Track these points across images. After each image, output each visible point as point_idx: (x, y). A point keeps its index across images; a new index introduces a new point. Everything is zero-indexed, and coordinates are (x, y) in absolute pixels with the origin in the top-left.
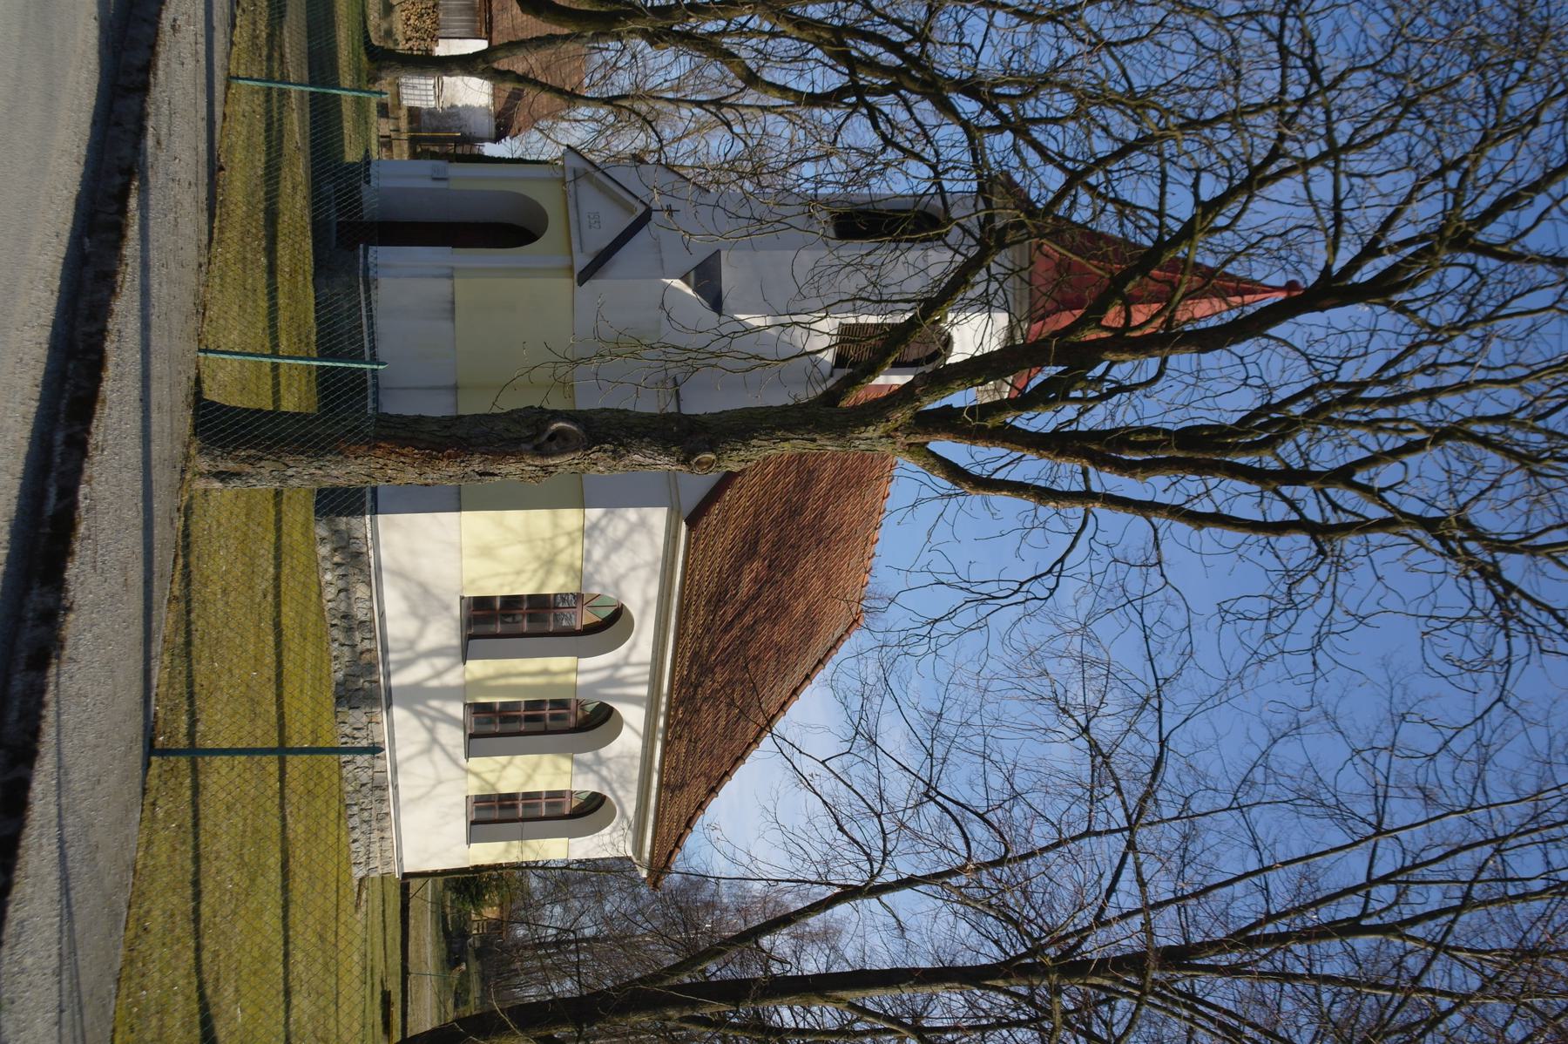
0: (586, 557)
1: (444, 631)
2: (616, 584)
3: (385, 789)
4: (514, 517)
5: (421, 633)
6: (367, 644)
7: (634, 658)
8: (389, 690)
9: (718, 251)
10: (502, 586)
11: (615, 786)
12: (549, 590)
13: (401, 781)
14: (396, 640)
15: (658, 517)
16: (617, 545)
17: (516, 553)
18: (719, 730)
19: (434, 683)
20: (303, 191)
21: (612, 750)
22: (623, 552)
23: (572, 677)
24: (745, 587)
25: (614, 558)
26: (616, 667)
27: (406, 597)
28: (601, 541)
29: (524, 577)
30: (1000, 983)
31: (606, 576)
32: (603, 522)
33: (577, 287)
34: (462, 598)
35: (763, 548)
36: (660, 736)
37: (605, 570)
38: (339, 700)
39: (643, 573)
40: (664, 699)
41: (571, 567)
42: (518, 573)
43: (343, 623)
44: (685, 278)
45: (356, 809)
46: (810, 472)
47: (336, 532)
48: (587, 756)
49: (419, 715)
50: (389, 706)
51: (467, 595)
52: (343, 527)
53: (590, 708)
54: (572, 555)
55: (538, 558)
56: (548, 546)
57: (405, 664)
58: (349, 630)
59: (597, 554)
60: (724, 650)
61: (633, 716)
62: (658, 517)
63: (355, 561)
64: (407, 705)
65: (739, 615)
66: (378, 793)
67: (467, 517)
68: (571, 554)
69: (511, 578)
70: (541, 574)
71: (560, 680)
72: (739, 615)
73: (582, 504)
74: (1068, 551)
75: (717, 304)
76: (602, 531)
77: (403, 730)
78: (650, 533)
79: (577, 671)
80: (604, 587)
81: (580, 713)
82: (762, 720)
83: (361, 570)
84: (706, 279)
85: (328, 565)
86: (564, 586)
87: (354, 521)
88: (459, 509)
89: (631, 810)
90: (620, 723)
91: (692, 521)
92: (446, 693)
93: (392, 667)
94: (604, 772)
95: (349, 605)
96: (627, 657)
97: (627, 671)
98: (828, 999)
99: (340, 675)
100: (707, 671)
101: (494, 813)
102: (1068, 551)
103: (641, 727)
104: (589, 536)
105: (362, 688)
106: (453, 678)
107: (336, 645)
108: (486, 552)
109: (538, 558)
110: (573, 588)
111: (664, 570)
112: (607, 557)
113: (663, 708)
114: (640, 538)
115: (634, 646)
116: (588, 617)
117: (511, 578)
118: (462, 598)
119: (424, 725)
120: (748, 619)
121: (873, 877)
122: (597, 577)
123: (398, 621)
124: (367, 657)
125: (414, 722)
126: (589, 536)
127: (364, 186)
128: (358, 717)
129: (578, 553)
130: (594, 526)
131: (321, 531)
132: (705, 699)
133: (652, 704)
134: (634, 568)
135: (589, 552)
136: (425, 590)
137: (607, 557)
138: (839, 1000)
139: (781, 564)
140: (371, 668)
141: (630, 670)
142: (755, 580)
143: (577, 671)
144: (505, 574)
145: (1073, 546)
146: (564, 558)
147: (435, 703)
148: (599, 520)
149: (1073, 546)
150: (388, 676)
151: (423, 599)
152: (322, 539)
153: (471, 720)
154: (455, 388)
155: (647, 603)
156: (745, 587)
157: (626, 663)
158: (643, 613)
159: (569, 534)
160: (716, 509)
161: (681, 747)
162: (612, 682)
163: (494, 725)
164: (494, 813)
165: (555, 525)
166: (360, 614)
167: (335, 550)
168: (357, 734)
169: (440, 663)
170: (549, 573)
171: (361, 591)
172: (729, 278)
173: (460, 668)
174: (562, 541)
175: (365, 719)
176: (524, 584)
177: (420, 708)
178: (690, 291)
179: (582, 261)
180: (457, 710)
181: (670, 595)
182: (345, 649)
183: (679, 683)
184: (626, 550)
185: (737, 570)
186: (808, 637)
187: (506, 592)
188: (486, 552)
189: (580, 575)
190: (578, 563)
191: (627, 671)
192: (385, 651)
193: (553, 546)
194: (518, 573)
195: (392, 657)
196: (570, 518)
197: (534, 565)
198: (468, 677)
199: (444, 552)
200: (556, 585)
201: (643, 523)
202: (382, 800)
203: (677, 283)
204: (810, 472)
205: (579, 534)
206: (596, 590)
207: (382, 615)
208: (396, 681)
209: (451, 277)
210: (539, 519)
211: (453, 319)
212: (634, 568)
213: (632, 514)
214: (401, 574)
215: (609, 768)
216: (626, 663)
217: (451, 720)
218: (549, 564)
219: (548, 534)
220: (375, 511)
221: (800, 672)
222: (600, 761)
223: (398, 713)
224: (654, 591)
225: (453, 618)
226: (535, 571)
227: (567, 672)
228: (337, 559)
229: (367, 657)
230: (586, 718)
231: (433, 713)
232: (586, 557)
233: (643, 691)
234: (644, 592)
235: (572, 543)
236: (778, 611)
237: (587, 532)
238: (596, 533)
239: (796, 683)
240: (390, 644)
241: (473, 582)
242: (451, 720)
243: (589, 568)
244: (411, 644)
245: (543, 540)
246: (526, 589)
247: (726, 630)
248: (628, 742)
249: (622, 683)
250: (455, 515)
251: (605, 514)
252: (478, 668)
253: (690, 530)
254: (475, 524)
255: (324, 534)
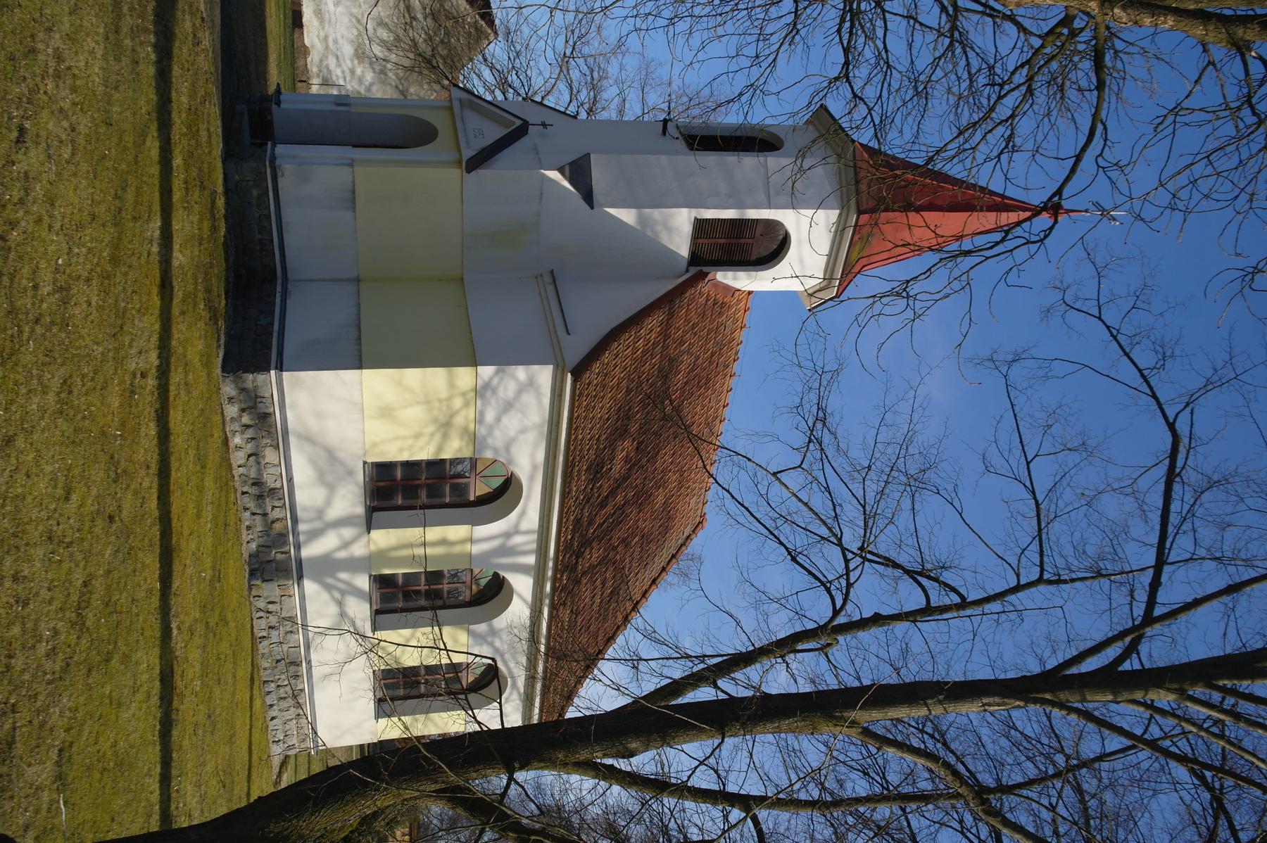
0: (480, 419)
1: (349, 500)
2: (507, 448)
3: (299, 664)
4: (413, 376)
5: (328, 502)
6: (277, 514)
7: (524, 526)
8: (299, 562)
9: (589, 154)
10: (401, 450)
11: (507, 656)
12: (447, 455)
13: (313, 657)
14: (305, 509)
15: (544, 375)
16: (508, 406)
17: (414, 414)
18: (595, 607)
19: (342, 554)
20: (208, 40)
21: (500, 622)
22: (513, 413)
23: (468, 547)
24: (618, 467)
25: (505, 420)
26: (507, 535)
27: (313, 461)
28: (493, 402)
29: (423, 440)
30: (1048, 696)
31: (497, 440)
32: (495, 381)
33: (465, 174)
34: (365, 463)
35: (634, 428)
36: (547, 601)
37: (497, 433)
38: (252, 574)
39: (531, 437)
40: (551, 564)
41: (465, 430)
42: (417, 436)
43: (254, 490)
44: (561, 170)
45: (273, 685)
46: (671, 361)
47: (243, 390)
48: (481, 628)
49: (328, 588)
50: (300, 578)
51: (369, 460)
52: (249, 385)
53: (483, 582)
54: (466, 418)
55: (435, 420)
56: (444, 408)
57: (315, 534)
58: (260, 497)
59: (490, 416)
60: (601, 525)
61: (522, 585)
62: (544, 375)
63: (263, 422)
64: (318, 579)
65: (613, 493)
66: (292, 669)
67: (367, 373)
68: (465, 417)
69: (410, 442)
70: (438, 437)
71: (457, 549)
72: (613, 493)
73: (474, 362)
74: (1068, 179)
75: (588, 198)
76: (494, 391)
77: (316, 602)
78: (539, 395)
79: (471, 540)
80: (496, 450)
81: (474, 587)
82: (629, 606)
83: (269, 433)
84: (579, 172)
85: (236, 427)
86: (460, 450)
87: (261, 378)
88: (360, 367)
89: (521, 683)
90: (511, 591)
91: (577, 373)
92: (353, 565)
93: (302, 538)
94: (498, 643)
95: (259, 470)
96: (517, 525)
97: (518, 540)
98: (839, 721)
99: (254, 546)
100: (586, 543)
101: (398, 688)
102: (1068, 179)
103: (528, 595)
104: (482, 397)
105: (274, 562)
106: (359, 550)
107: (248, 514)
108: (386, 413)
109: (435, 420)
110: (467, 453)
111: (550, 432)
112: (498, 420)
113: (550, 573)
114: (528, 398)
115: (523, 513)
116: (479, 488)
117: (410, 442)
118: (365, 463)
119: (333, 598)
120: (619, 499)
121: (836, 613)
122: (490, 441)
123: (307, 494)
124: (277, 526)
125: (325, 596)
126: (482, 397)
127: (274, 106)
128: (270, 590)
129: (472, 415)
130: (487, 386)
131: (229, 389)
132: (584, 573)
133: (538, 573)
134: (523, 431)
135: (482, 413)
136: (331, 454)
137: (498, 420)
138: (854, 723)
139: (645, 453)
140: (283, 536)
141: (515, 539)
142: (627, 460)
143: (471, 540)
144: (404, 438)
145: (1073, 170)
146: (459, 420)
147: (344, 576)
148: (491, 379)
149: (1073, 170)
150: (298, 547)
151: (330, 465)
152: (230, 399)
153: (376, 596)
154: (358, 280)
155: (535, 468)
156: (618, 467)
157: (516, 531)
158: (532, 478)
159: (464, 394)
160: (596, 367)
161: (565, 614)
162: (505, 551)
163: (401, 597)
164: (398, 688)
165: (451, 385)
166: (270, 482)
167: (243, 410)
168: (271, 608)
169: (348, 532)
170: (445, 436)
171: (270, 456)
172: (599, 177)
173: (365, 539)
174: (458, 403)
175: (278, 592)
176: (422, 448)
177: (330, 580)
178: (566, 184)
179: (467, 153)
180: (363, 582)
181: (555, 457)
182: (258, 518)
183: (563, 547)
184: (515, 415)
185: (612, 445)
186: (666, 529)
187: (405, 457)
188: (386, 413)
189: (474, 438)
190: (472, 426)
191: (518, 540)
192: (295, 521)
193: (449, 407)
194: (417, 436)
195: (302, 527)
196: (465, 376)
197: (430, 429)
198: (373, 548)
199: (347, 415)
200: (454, 448)
201: (531, 383)
202: (296, 677)
203: (554, 175)
204: (671, 361)
205: (472, 394)
206: (489, 454)
207: (290, 480)
208: (306, 552)
209: (351, 165)
210: (433, 379)
211: (354, 209)
212: (523, 431)
213: (521, 372)
214: (308, 438)
215: (501, 639)
216: (516, 531)
217: (357, 592)
218: (445, 426)
219: (444, 394)
220: (280, 368)
221: (656, 568)
222: (494, 632)
223: (310, 586)
224: (540, 456)
225: (357, 484)
226: (432, 435)
227: (463, 542)
228: (246, 419)
229: (278, 527)
230: (480, 592)
231: (342, 586)
232: (480, 419)
233: (531, 560)
234: (533, 456)
235: (467, 404)
236: (642, 498)
237: (481, 392)
238: (489, 393)
239: (655, 574)
240: (300, 514)
241: (374, 445)
242: (357, 592)
243: (482, 431)
244: (320, 513)
245: (440, 400)
246: (424, 453)
247: (603, 505)
248: (518, 611)
249: (512, 551)
250: (357, 372)
251: (497, 373)
252: (382, 538)
253: (575, 381)
254: (376, 384)
255: (233, 393)
